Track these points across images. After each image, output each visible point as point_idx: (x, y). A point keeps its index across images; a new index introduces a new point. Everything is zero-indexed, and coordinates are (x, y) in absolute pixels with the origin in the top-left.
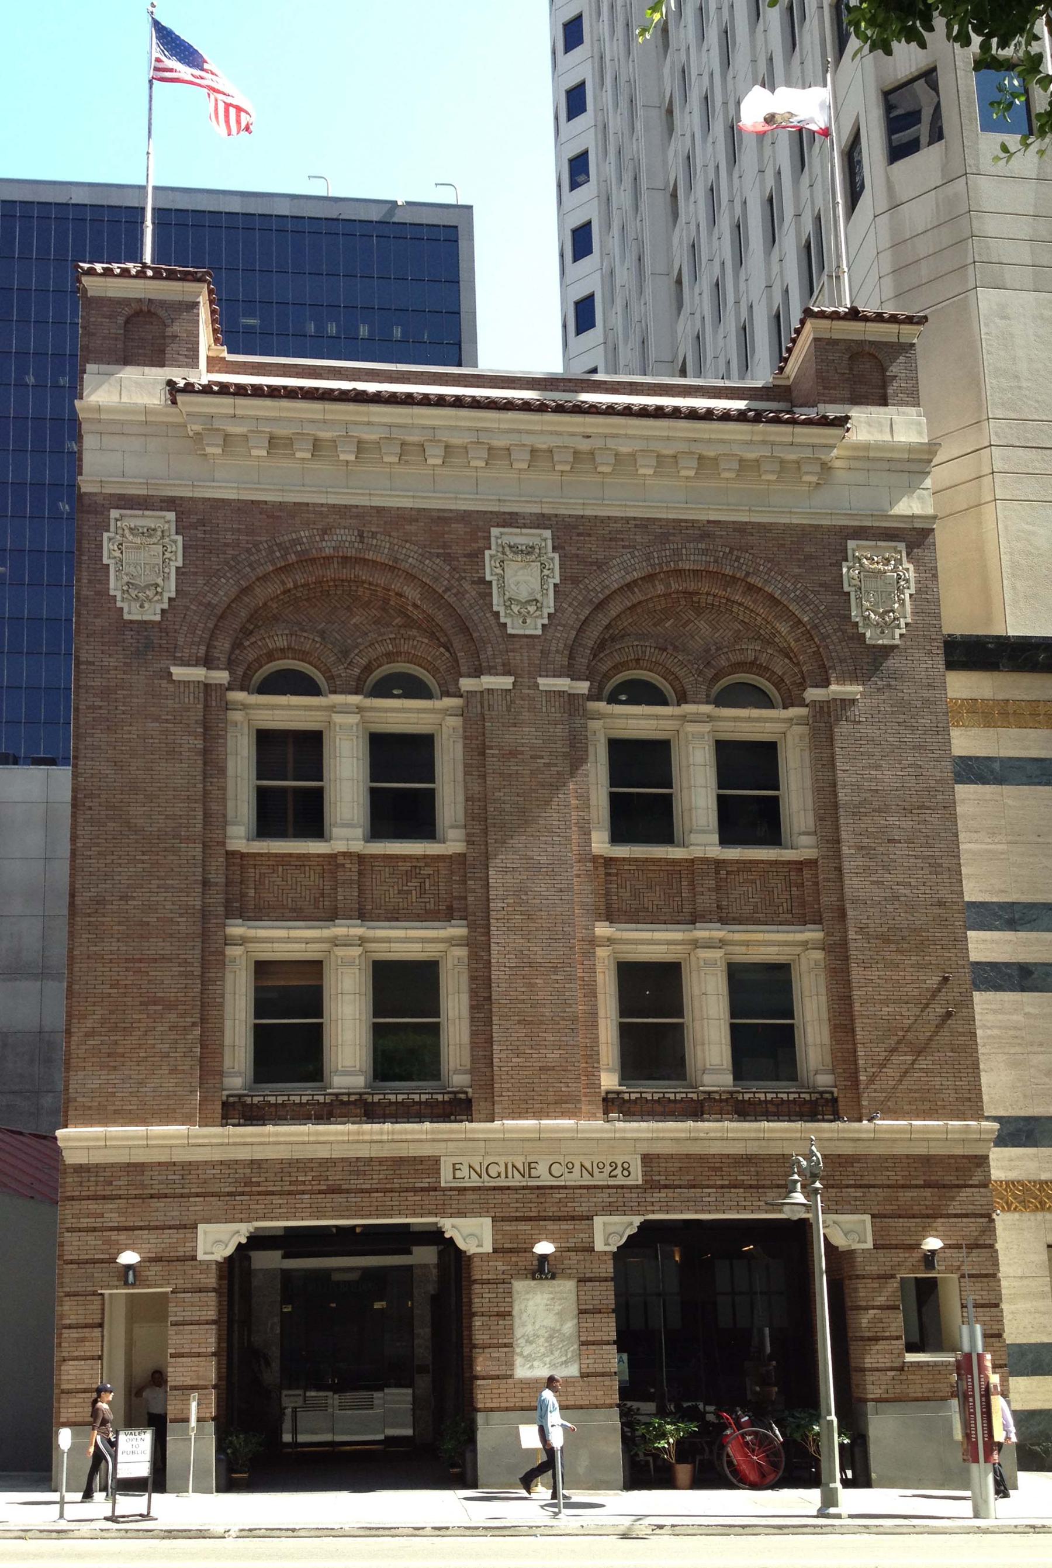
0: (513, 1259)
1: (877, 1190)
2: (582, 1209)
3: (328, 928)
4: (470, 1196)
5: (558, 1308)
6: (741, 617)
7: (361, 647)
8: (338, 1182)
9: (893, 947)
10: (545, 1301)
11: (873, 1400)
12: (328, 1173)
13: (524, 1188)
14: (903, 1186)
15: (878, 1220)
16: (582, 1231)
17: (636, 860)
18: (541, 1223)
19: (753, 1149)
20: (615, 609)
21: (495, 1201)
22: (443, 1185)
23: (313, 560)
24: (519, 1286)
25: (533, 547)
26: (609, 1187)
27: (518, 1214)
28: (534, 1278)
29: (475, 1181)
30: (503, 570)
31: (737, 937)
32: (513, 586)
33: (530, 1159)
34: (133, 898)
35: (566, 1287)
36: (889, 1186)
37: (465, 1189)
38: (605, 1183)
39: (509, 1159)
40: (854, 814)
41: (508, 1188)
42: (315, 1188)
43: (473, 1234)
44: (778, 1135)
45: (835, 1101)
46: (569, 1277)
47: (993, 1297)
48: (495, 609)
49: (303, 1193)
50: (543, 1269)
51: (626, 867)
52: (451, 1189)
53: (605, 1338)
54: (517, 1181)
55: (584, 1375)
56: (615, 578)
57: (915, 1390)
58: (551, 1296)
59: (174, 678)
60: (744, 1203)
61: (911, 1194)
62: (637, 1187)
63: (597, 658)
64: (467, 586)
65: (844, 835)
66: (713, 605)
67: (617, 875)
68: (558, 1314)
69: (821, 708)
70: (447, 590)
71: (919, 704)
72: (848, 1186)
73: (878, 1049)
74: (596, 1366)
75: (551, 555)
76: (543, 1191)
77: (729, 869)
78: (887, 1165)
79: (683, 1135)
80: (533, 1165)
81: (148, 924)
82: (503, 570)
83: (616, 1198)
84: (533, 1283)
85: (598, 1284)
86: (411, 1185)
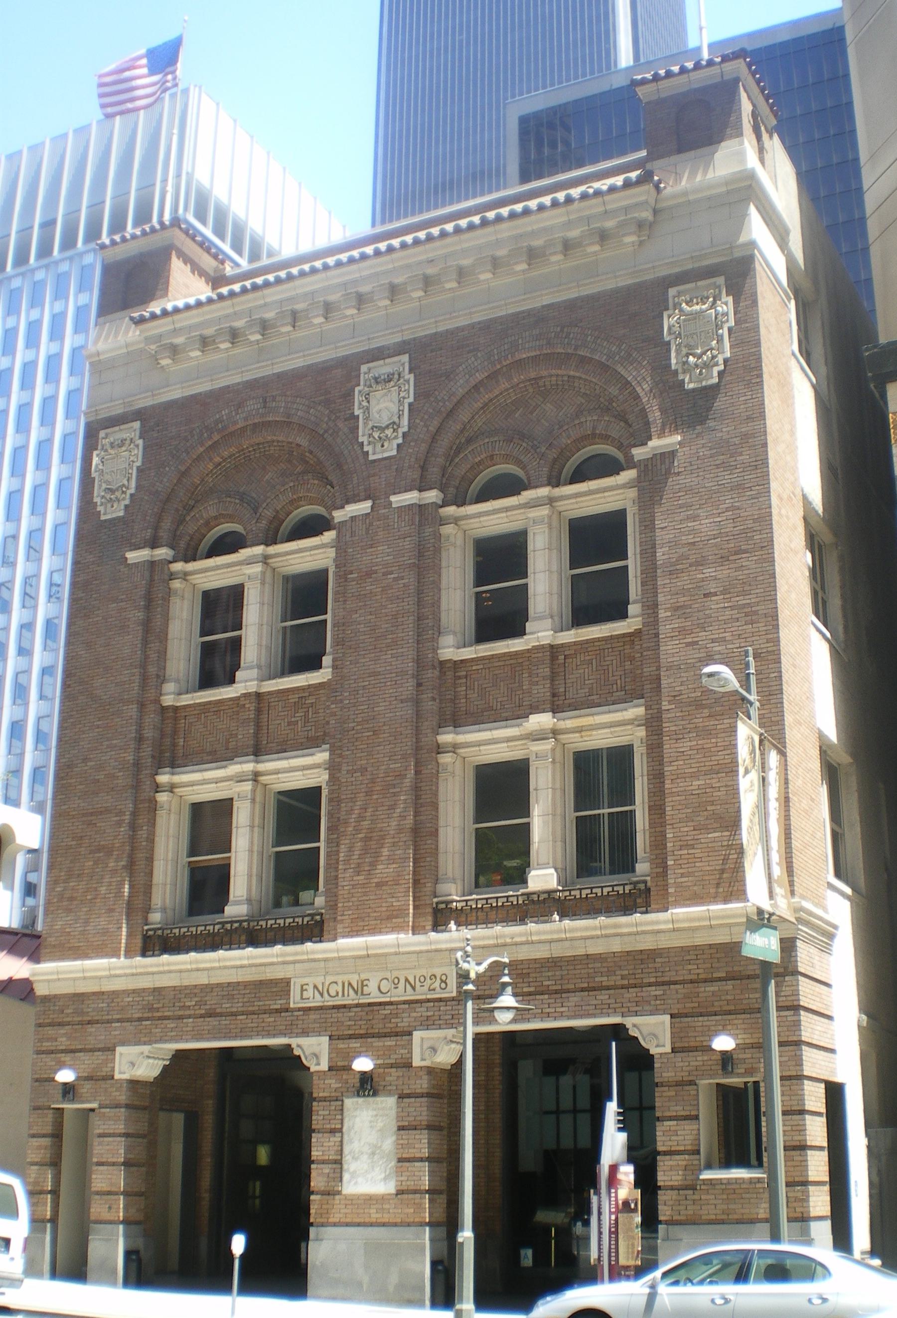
0: (344, 1077)
1: (677, 986)
2: (403, 1024)
3: (225, 767)
4: (313, 1016)
5: (380, 1125)
6: (583, 390)
7: (269, 500)
8: (213, 1007)
9: (706, 712)
10: (369, 1118)
11: (667, 1223)
12: (206, 998)
13: (357, 1005)
14: (705, 981)
15: (678, 1020)
16: (403, 1047)
17: (483, 658)
18: (369, 1040)
19: (558, 951)
20: (464, 415)
21: (332, 1020)
22: (292, 1006)
23: (232, 434)
24: (349, 1102)
25: (393, 374)
26: (429, 1001)
27: (350, 1032)
28: (358, 1095)
29: (317, 1001)
30: (368, 402)
31: (569, 724)
32: (375, 414)
33: (363, 976)
34: (90, 760)
35: (388, 1103)
36: (692, 982)
37: (310, 1009)
38: (424, 997)
39: (346, 978)
40: (671, 573)
41: (344, 1006)
42: (197, 1012)
43: (314, 1051)
44: (579, 934)
45: (648, 890)
46: (390, 1094)
47: (795, 1103)
48: (360, 440)
49: (189, 1017)
50: (367, 1085)
51: (474, 668)
52: (299, 1009)
53: (418, 1155)
54: (351, 999)
55: (399, 1192)
56: (460, 386)
57: (709, 1212)
58: (375, 1113)
59: (129, 562)
60: (548, 1010)
61: (712, 989)
62: (453, 999)
63: (453, 464)
64: (340, 424)
65: (661, 598)
66: (557, 385)
67: (466, 677)
68: (380, 1130)
69: (646, 466)
70: (326, 431)
71: (737, 441)
72: (650, 985)
73: (686, 829)
74: (409, 1183)
75: (407, 377)
76: (371, 1008)
77: (566, 653)
78: (688, 958)
79: (491, 942)
80: (365, 983)
81: (98, 781)
82: (368, 402)
83: (442, 1012)
84: (361, 1100)
85: (413, 1100)
86: (267, 1008)
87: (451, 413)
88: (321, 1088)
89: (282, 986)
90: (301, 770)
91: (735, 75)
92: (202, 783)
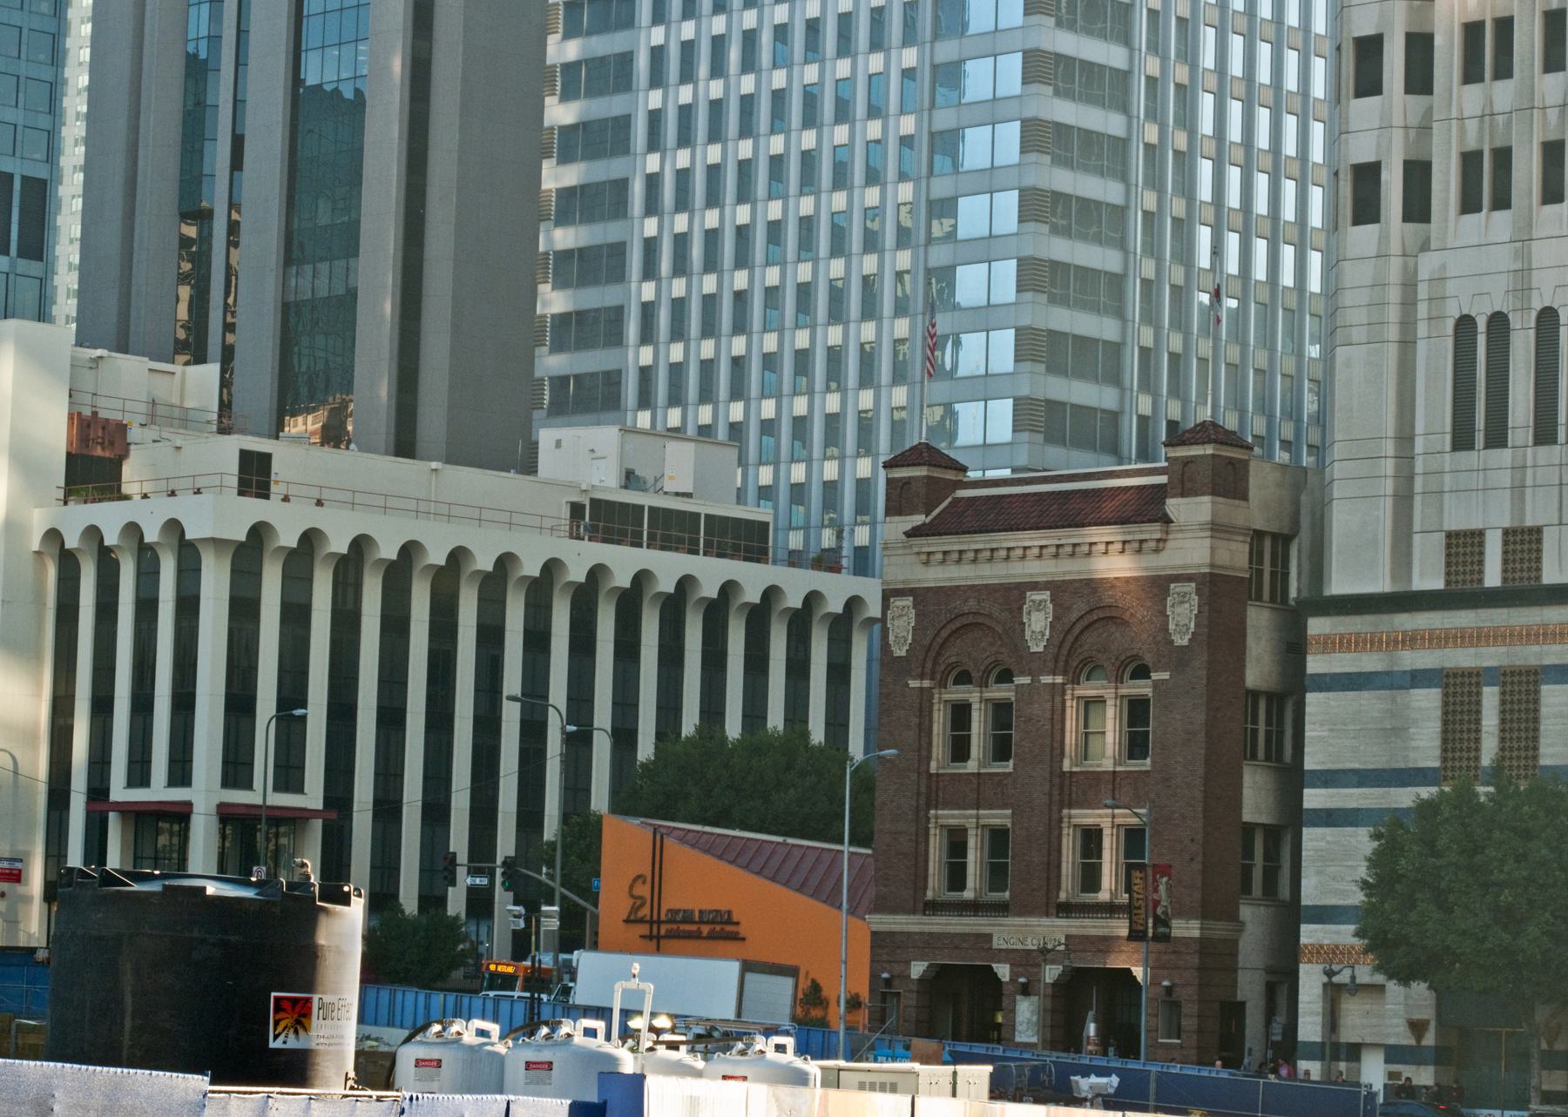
43: (1003, 971)
56: (1075, 615)
87: (1069, 631)
88: (1006, 990)
89: (988, 937)
90: (1000, 817)
91: (1507, 14)
92: (951, 816)
